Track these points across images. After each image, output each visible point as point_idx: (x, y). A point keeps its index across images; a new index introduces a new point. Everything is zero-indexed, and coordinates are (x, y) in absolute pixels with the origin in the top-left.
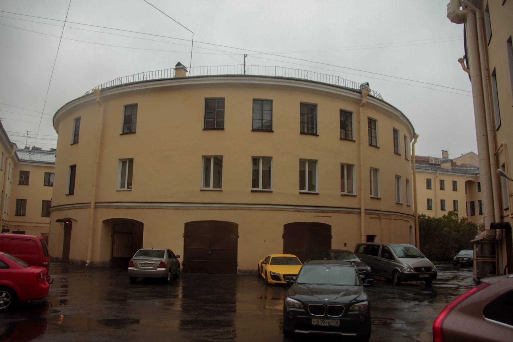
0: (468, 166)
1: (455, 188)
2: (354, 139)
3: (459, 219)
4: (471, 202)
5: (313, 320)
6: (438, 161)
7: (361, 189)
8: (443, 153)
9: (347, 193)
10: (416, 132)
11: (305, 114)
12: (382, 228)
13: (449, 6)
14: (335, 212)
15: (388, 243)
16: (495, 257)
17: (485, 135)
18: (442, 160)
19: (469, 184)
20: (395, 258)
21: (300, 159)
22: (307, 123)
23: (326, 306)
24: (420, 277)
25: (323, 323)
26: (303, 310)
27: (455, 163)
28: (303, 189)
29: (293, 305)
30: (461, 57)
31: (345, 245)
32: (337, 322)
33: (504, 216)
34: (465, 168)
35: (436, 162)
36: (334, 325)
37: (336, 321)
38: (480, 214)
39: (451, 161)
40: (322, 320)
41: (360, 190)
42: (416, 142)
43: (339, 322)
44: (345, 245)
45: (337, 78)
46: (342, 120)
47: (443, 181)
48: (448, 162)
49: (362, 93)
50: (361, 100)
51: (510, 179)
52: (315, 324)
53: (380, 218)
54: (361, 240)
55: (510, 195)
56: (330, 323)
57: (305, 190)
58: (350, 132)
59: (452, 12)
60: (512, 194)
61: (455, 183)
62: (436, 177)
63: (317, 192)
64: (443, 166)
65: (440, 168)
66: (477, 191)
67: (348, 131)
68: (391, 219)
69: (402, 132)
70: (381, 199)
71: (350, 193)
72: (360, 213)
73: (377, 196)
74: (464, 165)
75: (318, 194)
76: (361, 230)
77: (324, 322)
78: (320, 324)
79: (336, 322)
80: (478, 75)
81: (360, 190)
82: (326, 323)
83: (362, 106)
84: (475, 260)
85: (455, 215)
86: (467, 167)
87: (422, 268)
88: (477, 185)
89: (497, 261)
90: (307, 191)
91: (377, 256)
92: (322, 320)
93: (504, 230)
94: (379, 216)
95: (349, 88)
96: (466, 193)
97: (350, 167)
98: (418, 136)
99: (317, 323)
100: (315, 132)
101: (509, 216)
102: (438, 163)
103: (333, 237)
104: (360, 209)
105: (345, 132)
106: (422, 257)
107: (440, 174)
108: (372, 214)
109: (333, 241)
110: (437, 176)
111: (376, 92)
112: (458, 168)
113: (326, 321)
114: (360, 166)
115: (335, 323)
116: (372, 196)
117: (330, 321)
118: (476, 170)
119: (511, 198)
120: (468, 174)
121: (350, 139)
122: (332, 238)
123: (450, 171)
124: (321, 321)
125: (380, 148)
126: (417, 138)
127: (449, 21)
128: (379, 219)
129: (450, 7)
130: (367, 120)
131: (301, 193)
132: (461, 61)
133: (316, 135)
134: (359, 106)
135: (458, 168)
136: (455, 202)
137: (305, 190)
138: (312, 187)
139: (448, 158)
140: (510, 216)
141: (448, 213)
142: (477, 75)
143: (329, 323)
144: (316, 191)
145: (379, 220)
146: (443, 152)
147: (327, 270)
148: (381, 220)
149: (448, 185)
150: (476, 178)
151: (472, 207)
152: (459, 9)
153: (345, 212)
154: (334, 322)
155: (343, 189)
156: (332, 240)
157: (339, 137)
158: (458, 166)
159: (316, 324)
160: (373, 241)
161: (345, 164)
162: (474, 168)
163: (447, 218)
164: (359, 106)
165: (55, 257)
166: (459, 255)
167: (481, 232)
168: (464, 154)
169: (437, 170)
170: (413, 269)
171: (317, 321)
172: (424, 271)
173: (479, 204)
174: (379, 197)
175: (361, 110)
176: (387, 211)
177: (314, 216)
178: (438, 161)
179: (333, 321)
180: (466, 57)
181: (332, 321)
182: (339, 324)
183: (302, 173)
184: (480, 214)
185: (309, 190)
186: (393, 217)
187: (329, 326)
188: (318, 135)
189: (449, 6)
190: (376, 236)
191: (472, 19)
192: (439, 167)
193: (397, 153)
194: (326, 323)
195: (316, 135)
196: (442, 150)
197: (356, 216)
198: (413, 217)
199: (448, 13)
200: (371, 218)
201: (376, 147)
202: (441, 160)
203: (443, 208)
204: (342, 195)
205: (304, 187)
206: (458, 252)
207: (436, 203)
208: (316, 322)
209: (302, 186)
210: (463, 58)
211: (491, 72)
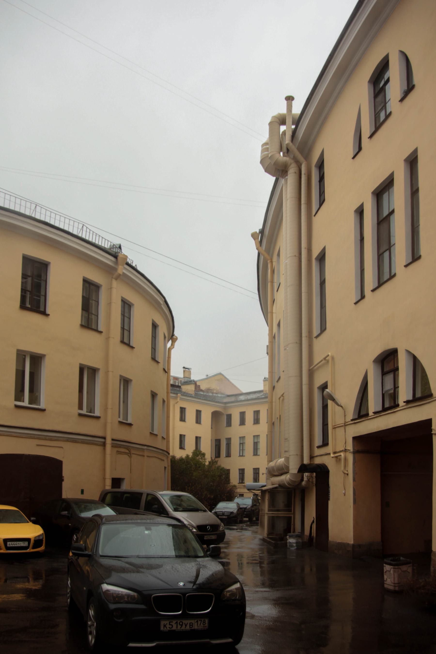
0: (215, 391)
1: (198, 421)
2: (100, 329)
3: (206, 462)
4: (216, 440)
5: (163, 623)
6: (177, 381)
7: (107, 408)
8: (184, 371)
9: (87, 412)
10: (176, 333)
11: (29, 276)
12: (132, 469)
13: (265, 147)
14: (68, 440)
15: (155, 490)
16: (291, 510)
17: (298, 342)
18: (183, 380)
19: (216, 415)
20: (169, 513)
21: (18, 351)
22: (31, 292)
23: (184, 594)
24: (205, 539)
25: (180, 626)
26: (143, 607)
27: (199, 386)
28: (20, 401)
29: (118, 598)
30: (256, 231)
31: (82, 492)
32: (203, 622)
33: (315, 455)
34: (211, 394)
35: (175, 382)
36: (199, 628)
37: (203, 620)
38: (226, 457)
39: (195, 383)
40: (179, 622)
41: (105, 409)
42: (174, 348)
43: (207, 621)
44: (82, 492)
45: (81, 226)
46: (84, 295)
47: (184, 410)
48: (192, 384)
49: (119, 258)
50: (115, 269)
51: (340, 404)
52: (165, 629)
53: (130, 454)
54: (105, 486)
55: (334, 427)
56: (192, 625)
57: (23, 401)
58: (93, 317)
59: (269, 156)
60: (335, 426)
61: (198, 413)
62: (176, 403)
63: (42, 406)
64: (186, 388)
65: (180, 391)
66: (225, 426)
67: (92, 314)
68: (144, 456)
69: (162, 330)
70: (133, 425)
71: (90, 412)
72: (104, 445)
73: (127, 420)
74: (210, 390)
75: (43, 410)
76: (104, 470)
77: (182, 625)
78: (174, 628)
79: (202, 622)
80: (296, 255)
81: (105, 409)
82: (186, 626)
83: (116, 279)
84: (266, 514)
85: (201, 456)
86: (213, 393)
87: (206, 526)
88: (225, 417)
89: (292, 516)
90: (26, 403)
91: (139, 509)
92: (179, 622)
93: (315, 474)
94: (129, 451)
95: (100, 245)
96: (212, 428)
97: (93, 371)
98: (177, 339)
99: (169, 628)
100: (42, 309)
101: (329, 454)
102: (177, 384)
103: (65, 479)
104: (104, 438)
105: (87, 315)
106: (205, 511)
107: (181, 399)
108: (120, 447)
109: (65, 485)
110: (178, 402)
111: (132, 261)
112: (202, 393)
113: (185, 622)
114: (107, 372)
115: (200, 625)
116: (121, 420)
117: (192, 621)
118: (224, 397)
119: (334, 430)
120: (216, 402)
121: (93, 327)
122: (63, 480)
123: (193, 395)
124: (177, 622)
125: (134, 348)
126: (175, 342)
127: (261, 169)
128: (129, 454)
129: (268, 148)
130: (120, 303)
131: (17, 407)
132: (254, 236)
133: (44, 313)
134: (112, 278)
135: (202, 393)
136: (198, 439)
137: (23, 401)
138: (34, 399)
139: (190, 378)
140: (332, 455)
141: (192, 453)
142: (295, 256)
143: (190, 625)
144: (40, 405)
145: (129, 456)
146: (184, 369)
147: (146, 532)
148: (130, 457)
149: (191, 415)
150: (225, 408)
151: (217, 446)
152: (280, 154)
153: (83, 442)
154: (199, 622)
155: (80, 407)
156: (64, 483)
157: (80, 322)
158: (202, 391)
159: (168, 629)
160: (119, 487)
161: (85, 366)
162: (222, 395)
163: (193, 459)
164: (112, 278)
165: (267, 462)
166: (218, 509)
167: (271, 478)
168: (210, 375)
169: (177, 394)
170: (196, 528)
171: (170, 624)
172: (210, 530)
173: (227, 443)
174: (129, 421)
175: (115, 283)
176: (139, 443)
177: (37, 445)
178: (177, 381)
179: (197, 621)
180: (262, 232)
181: (196, 621)
182: (207, 625)
183: (20, 374)
184: (226, 457)
185: (30, 403)
186: (146, 453)
187: (191, 630)
188: (49, 315)
189: (265, 147)
190: (123, 479)
191: (295, 173)
192: (178, 389)
193: (154, 359)
194: (186, 626)
195: (44, 313)
196: (183, 367)
197: (98, 449)
198: (165, 453)
199: (261, 157)
200: (118, 452)
201: (128, 345)
202: (181, 380)
203: (183, 446)
204: (80, 415)
205: (23, 397)
206: (216, 505)
207: (174, 439)
208: (168, 626)
209: (19, 396)
210: (258, 232)
211: (316, 253)
